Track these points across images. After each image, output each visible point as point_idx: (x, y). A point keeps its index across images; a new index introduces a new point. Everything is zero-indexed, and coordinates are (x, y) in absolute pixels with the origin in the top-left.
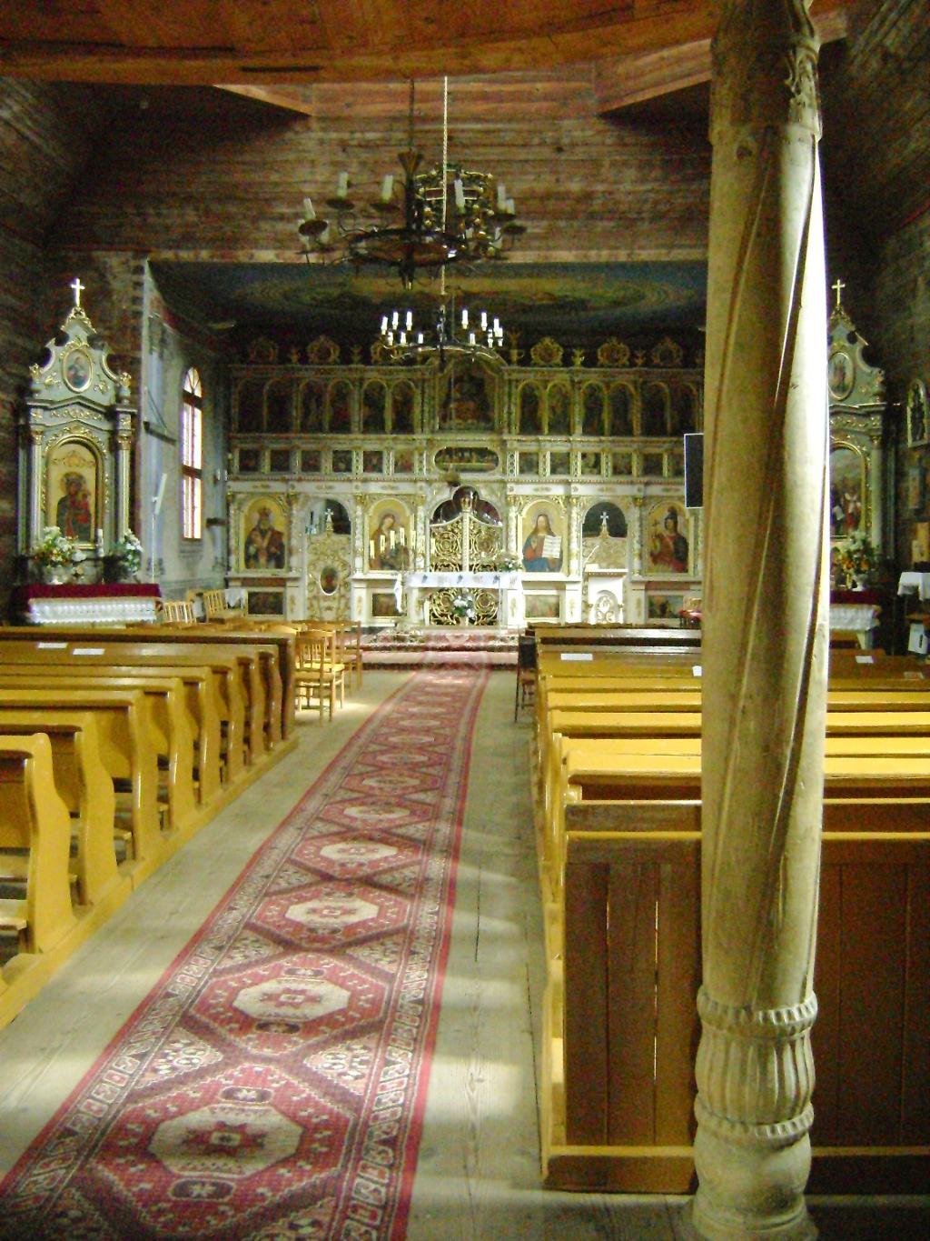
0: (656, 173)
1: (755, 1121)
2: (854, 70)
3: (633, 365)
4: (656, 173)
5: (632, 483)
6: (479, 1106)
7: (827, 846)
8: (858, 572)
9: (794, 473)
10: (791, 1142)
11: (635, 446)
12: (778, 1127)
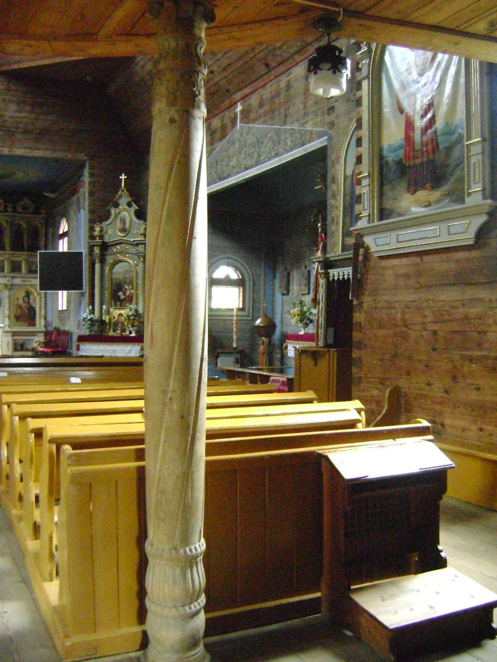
0: (27, 108)
1: (181, 605)
2: (138, 68)
3: (6, 211)
4: (27, 108)
5: (4, 277)
6: (10, 627)
7: (208, 463)
8: (133, 326)
9: (195, 280)
10: (197, 613)
11: (7, 256)
12: (192, 606)
